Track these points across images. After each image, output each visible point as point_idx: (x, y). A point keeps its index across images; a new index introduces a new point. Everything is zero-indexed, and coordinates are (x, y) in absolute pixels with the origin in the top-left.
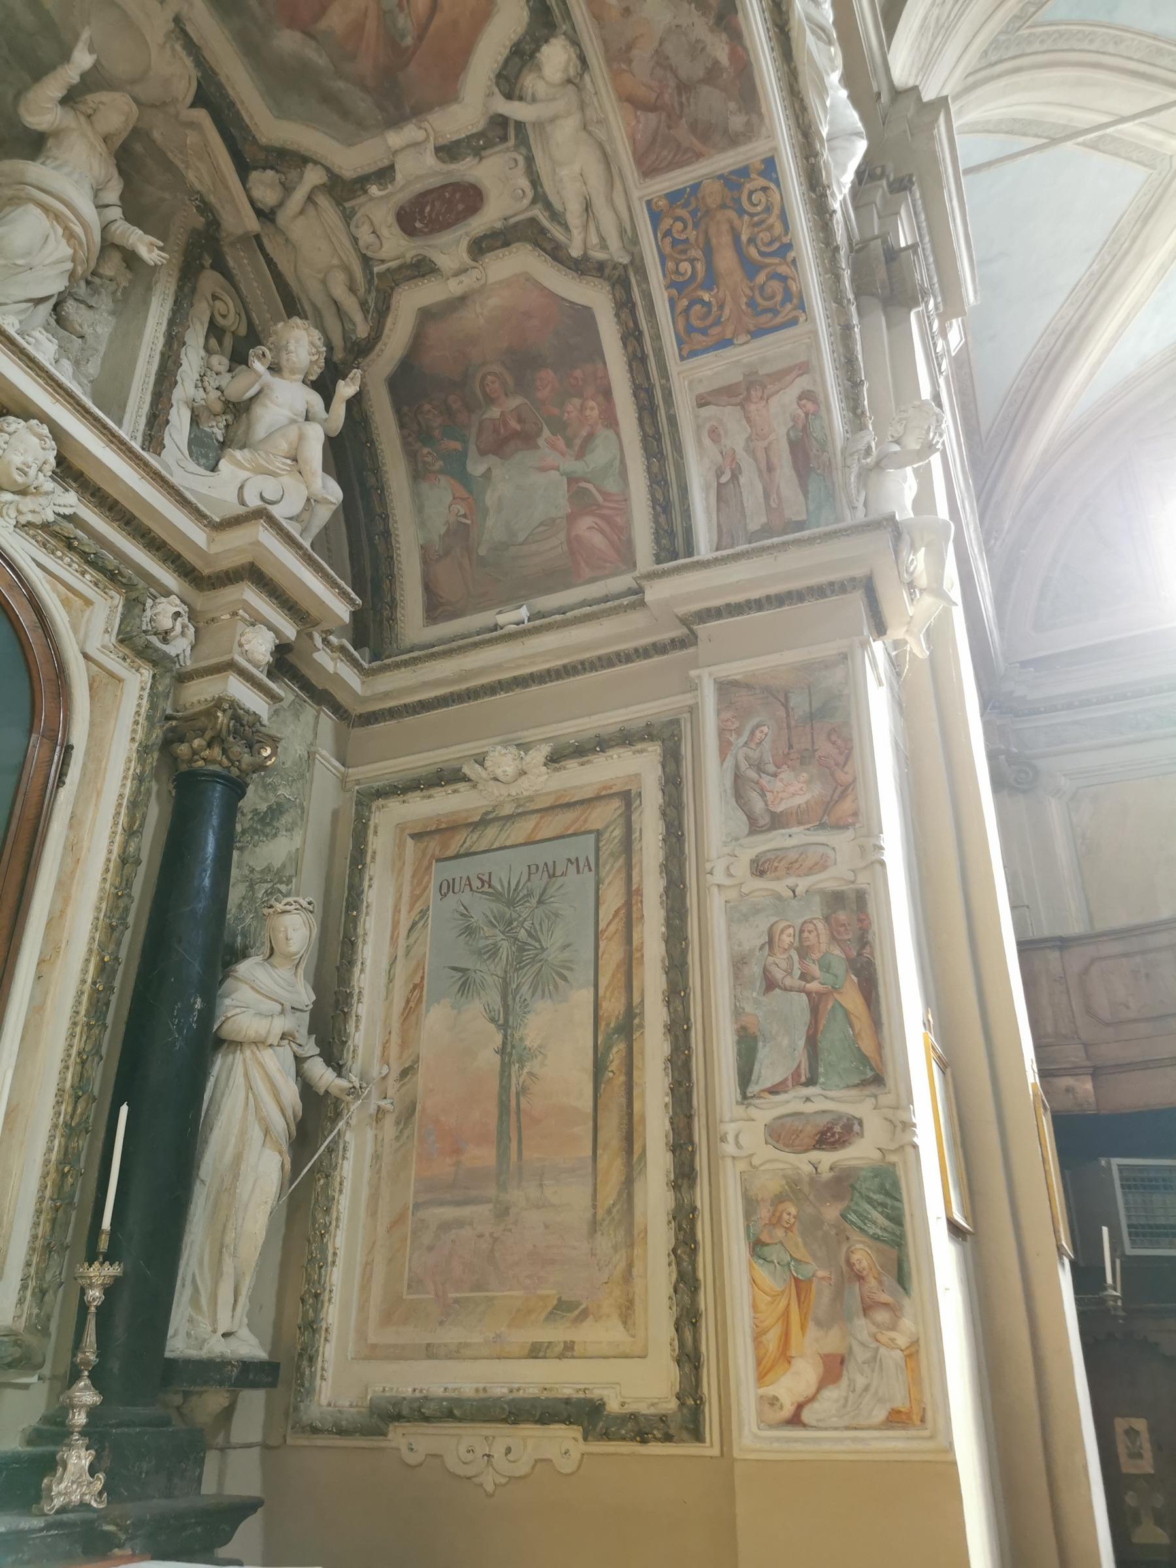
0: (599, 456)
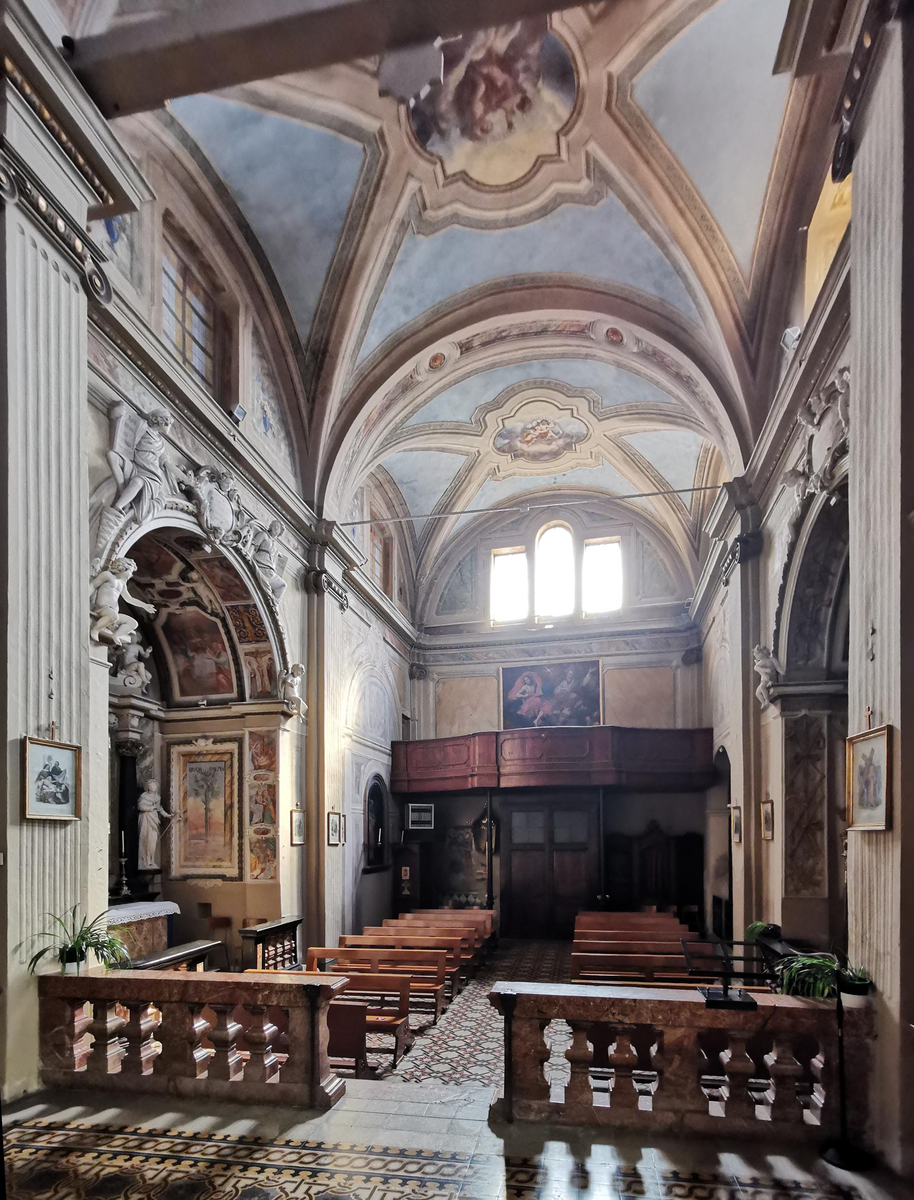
0: (222, 659)
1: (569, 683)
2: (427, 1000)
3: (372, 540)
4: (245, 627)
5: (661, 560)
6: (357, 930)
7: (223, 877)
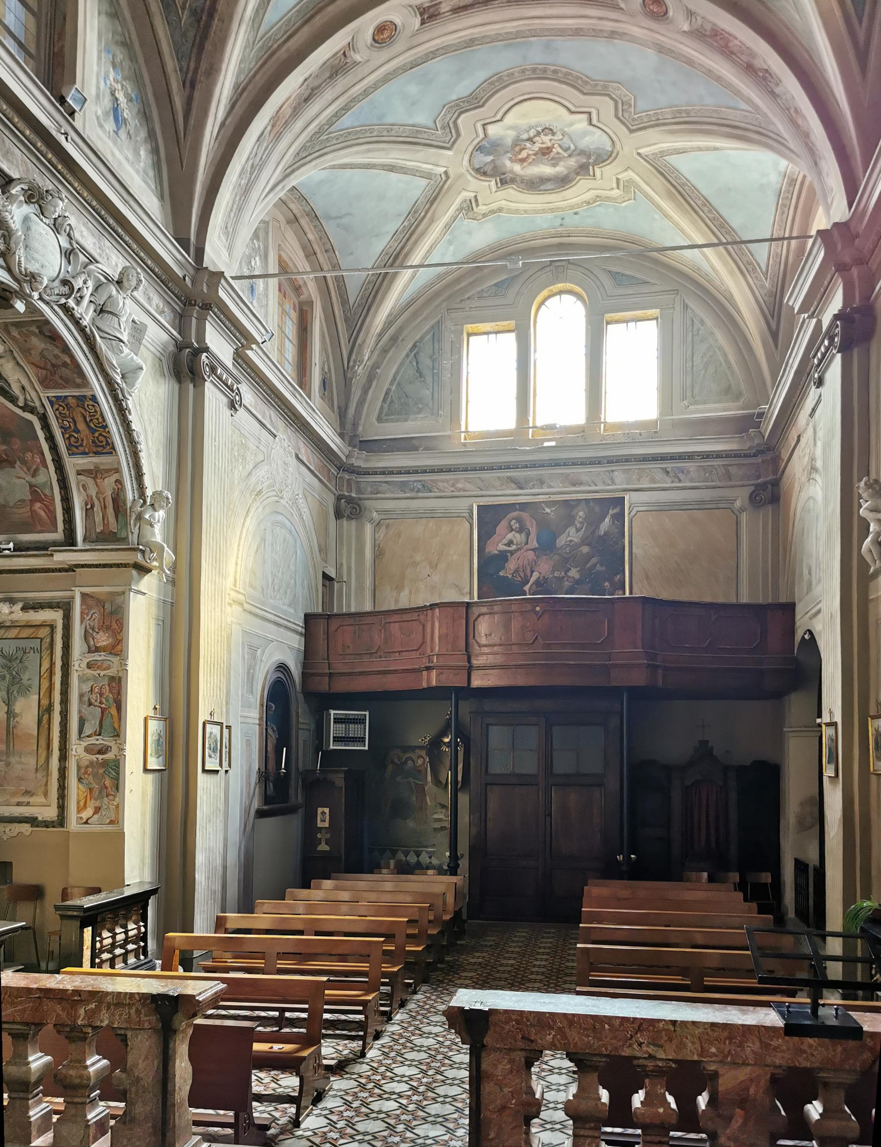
0: (41, 479)
1: (578, 530)
2: (352, 1017)
3: (281, 304)
4: (77, 431)
5: (721, 348)
6: (246, 905)
7: (32, 821)
